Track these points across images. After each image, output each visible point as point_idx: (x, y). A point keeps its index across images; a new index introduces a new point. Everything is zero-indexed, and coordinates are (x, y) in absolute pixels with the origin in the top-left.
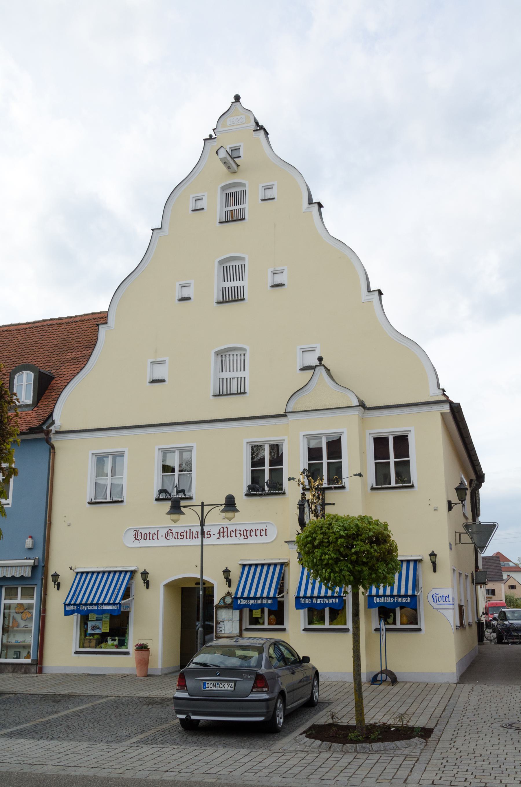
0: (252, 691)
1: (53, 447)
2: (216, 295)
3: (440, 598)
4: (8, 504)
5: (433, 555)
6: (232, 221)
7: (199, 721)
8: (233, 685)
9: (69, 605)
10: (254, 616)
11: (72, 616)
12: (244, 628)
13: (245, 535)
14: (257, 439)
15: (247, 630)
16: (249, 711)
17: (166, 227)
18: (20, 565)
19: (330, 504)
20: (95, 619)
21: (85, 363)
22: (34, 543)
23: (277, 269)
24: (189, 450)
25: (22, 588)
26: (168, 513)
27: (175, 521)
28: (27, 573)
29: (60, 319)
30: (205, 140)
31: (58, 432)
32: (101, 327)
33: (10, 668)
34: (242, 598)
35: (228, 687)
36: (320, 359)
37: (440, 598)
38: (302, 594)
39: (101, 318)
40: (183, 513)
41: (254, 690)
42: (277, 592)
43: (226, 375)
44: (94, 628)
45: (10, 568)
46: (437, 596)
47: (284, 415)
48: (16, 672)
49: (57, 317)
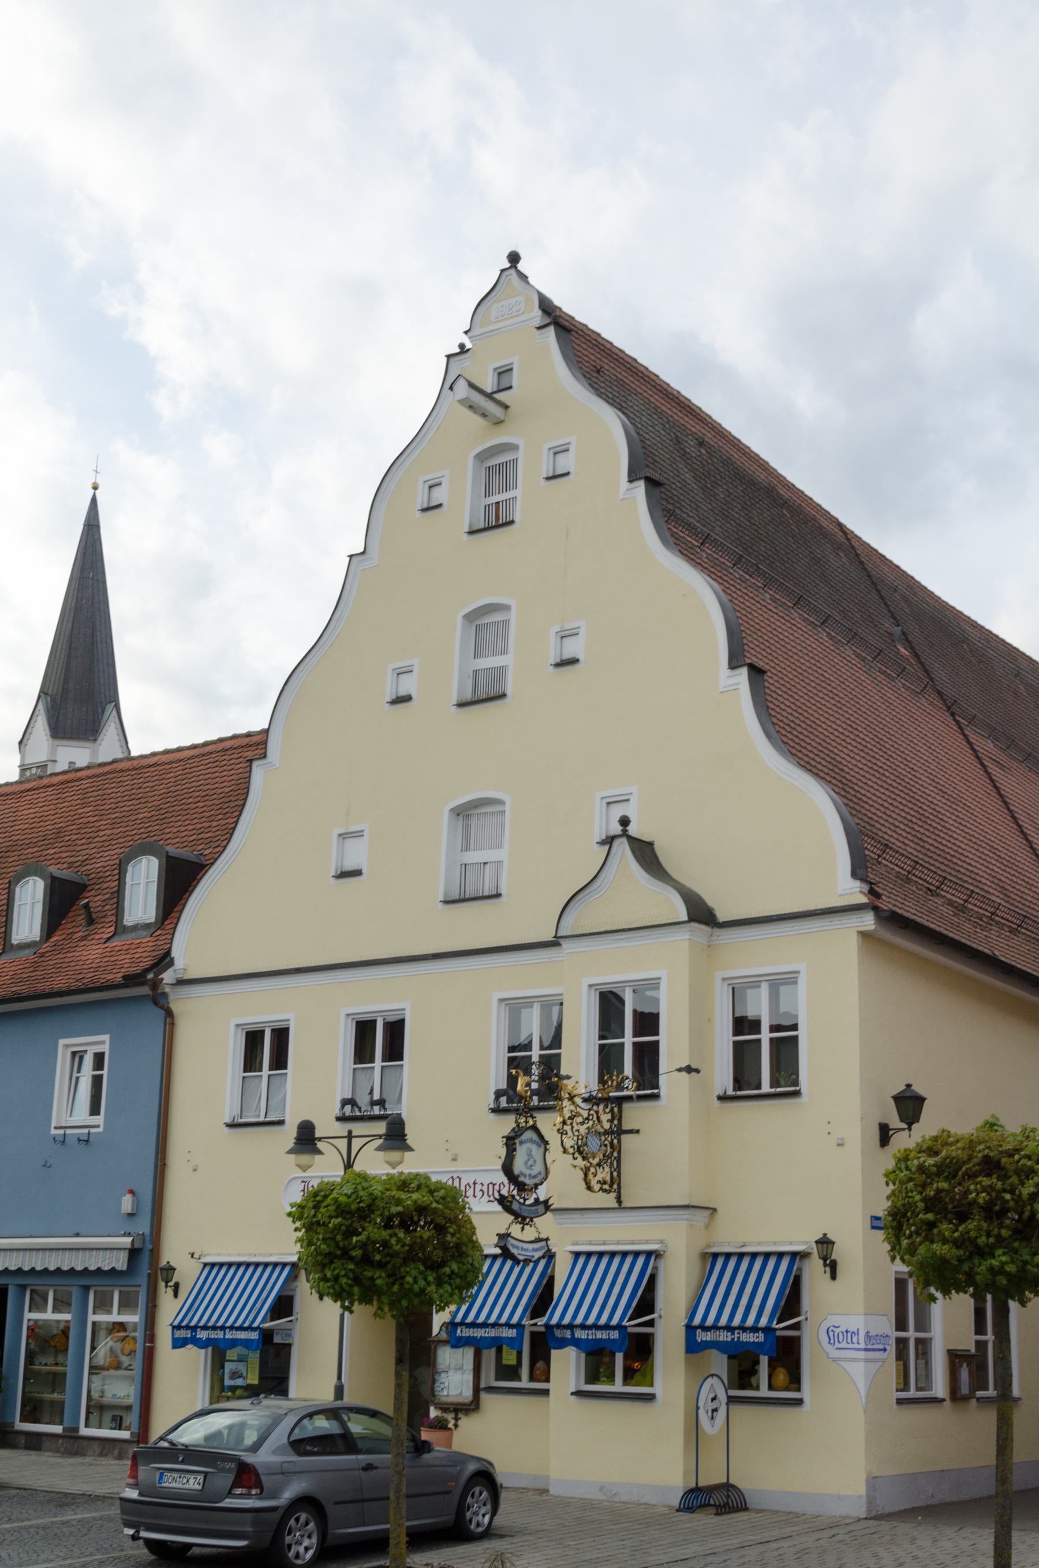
0: (230, 1493)
1: (169, 1013)
2: (454, 689)
3: (841, 1335)
4: (98, 1126)
5: (825, 1243)
6: (498, 526)
7: (189, 1546)
8: (201, 1481)
9: (178, 1327)
10: (504, 1362)
11: (183, 1349)
12: (483, 1385)
13: (491, 1193)
14: (609, 977)
15: (490, 1389)
16: (228, 1528)
17: (373, 550)
18: (107, 1248)
19: (631, 1132)
20: (235, 1358)
21: (224, 843)
22: (137, 1204)
23: (568, 626)
24: (654, 984)
25: (120, 1292)
26: (290, 1152)
27: (304, 1168)
28: (120, 1262)
29: (248, 735)
30: (449, 357)
31: (181, 982)
32: (255, 764)
33: (96, 1447)
34: (462, 1323)
35: (194, 1483)
36: (625, 822)
37: (841, 1335)
38: (697, 1321)
39: (251, 747)
40: (319, 1152)
41: (239, 1491)
42: (778, 1315)
43: (473, 857)
44: (235, 1375)
45: (94, 1252)
46: (837, 1330)
47: (554, 943)
48: (106, 1455)
49: (244, 731)
